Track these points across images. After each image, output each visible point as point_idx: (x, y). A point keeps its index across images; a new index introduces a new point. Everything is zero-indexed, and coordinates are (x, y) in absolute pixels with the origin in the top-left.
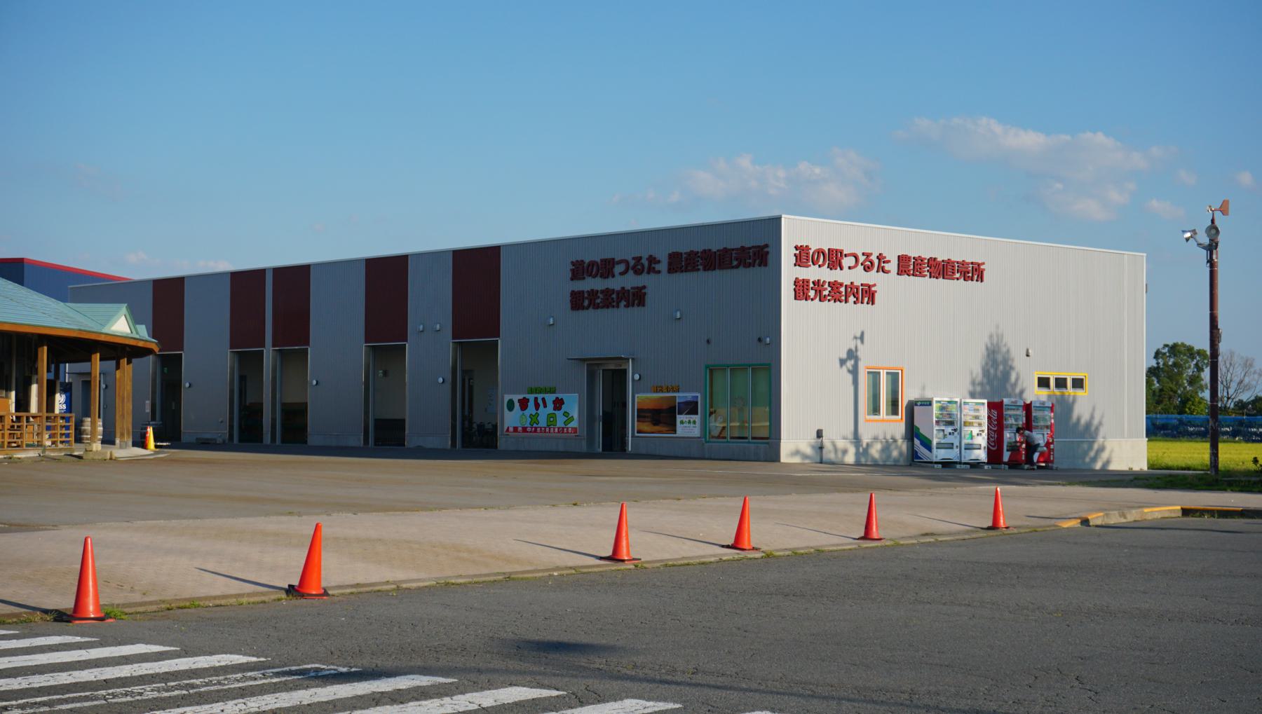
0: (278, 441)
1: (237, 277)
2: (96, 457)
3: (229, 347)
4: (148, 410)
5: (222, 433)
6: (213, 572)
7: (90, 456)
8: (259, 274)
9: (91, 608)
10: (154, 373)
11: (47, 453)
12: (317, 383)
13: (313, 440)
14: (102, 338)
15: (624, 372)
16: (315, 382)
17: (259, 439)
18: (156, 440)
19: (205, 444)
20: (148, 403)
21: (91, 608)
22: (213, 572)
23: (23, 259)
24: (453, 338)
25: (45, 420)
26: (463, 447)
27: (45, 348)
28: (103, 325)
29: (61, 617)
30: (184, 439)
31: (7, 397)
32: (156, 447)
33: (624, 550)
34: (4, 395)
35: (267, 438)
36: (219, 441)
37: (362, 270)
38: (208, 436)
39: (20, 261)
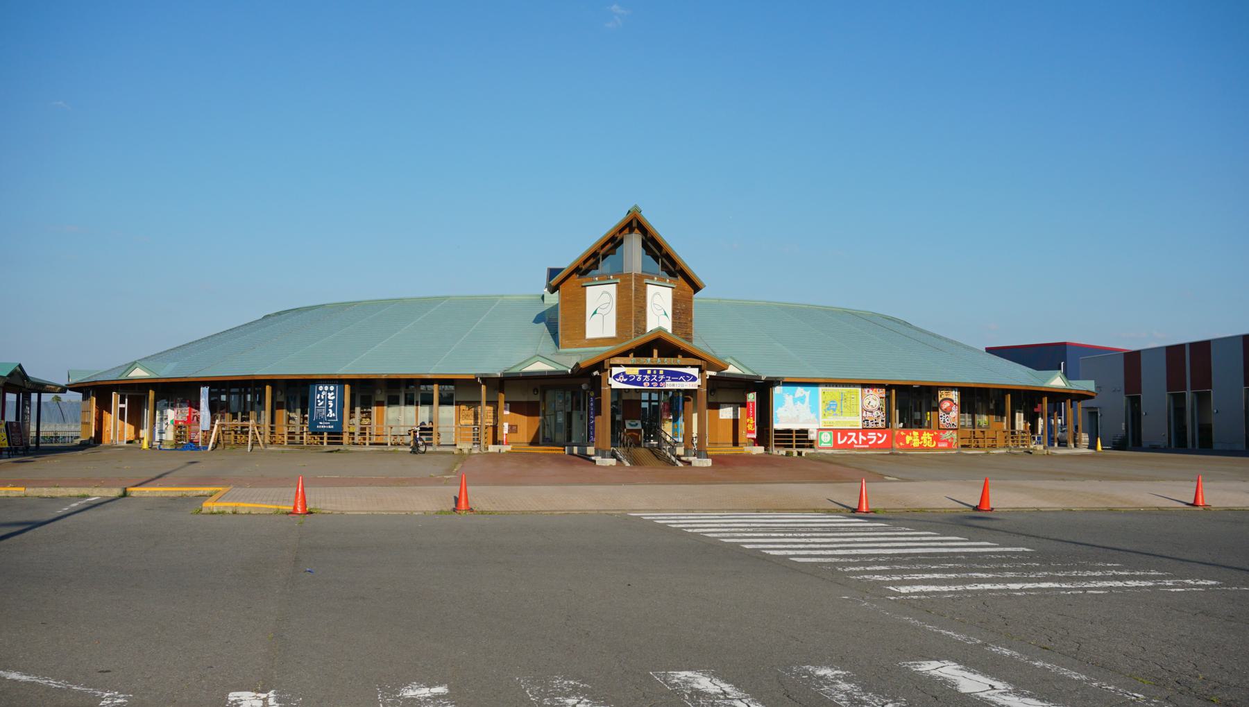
0: (1197, 447)
1: (1170, 349)
2: (1039, 453)
3: (1243, 385)
4: (1123, 429)
5: (1163, 442)
6: (957, 501)
7: (1036, 452)
8: (1182, 346)
9: (864, 508)
10: (1127, 407)
11: (1012, 451)
12: (1217, 412)
13: (1216, 446)
14: (1043, 389)
15: (1097, 413)
16: (1215, 411)
17: (1186, 446)
18: (1102, 445)
19: (1154, 449)
20: (1123, 424)
21: (864, 508)
22: (957, 501)
23: (1064, 344)
24: (1168, 391)
25: (1010, 434)
26: (1200, 447)
27: (1009, 395)
28: (1044, 382)
29: (854, 511)
30: (1144, 445)
31: (1002, 421)
32: (1103, 449)
33: (1200, 501)
34: (1000, 420)
35: (1190, 445)
36: (1162, 447)
37: (1240, 344)
38: (1156, 444)
39: (1062, 346)
